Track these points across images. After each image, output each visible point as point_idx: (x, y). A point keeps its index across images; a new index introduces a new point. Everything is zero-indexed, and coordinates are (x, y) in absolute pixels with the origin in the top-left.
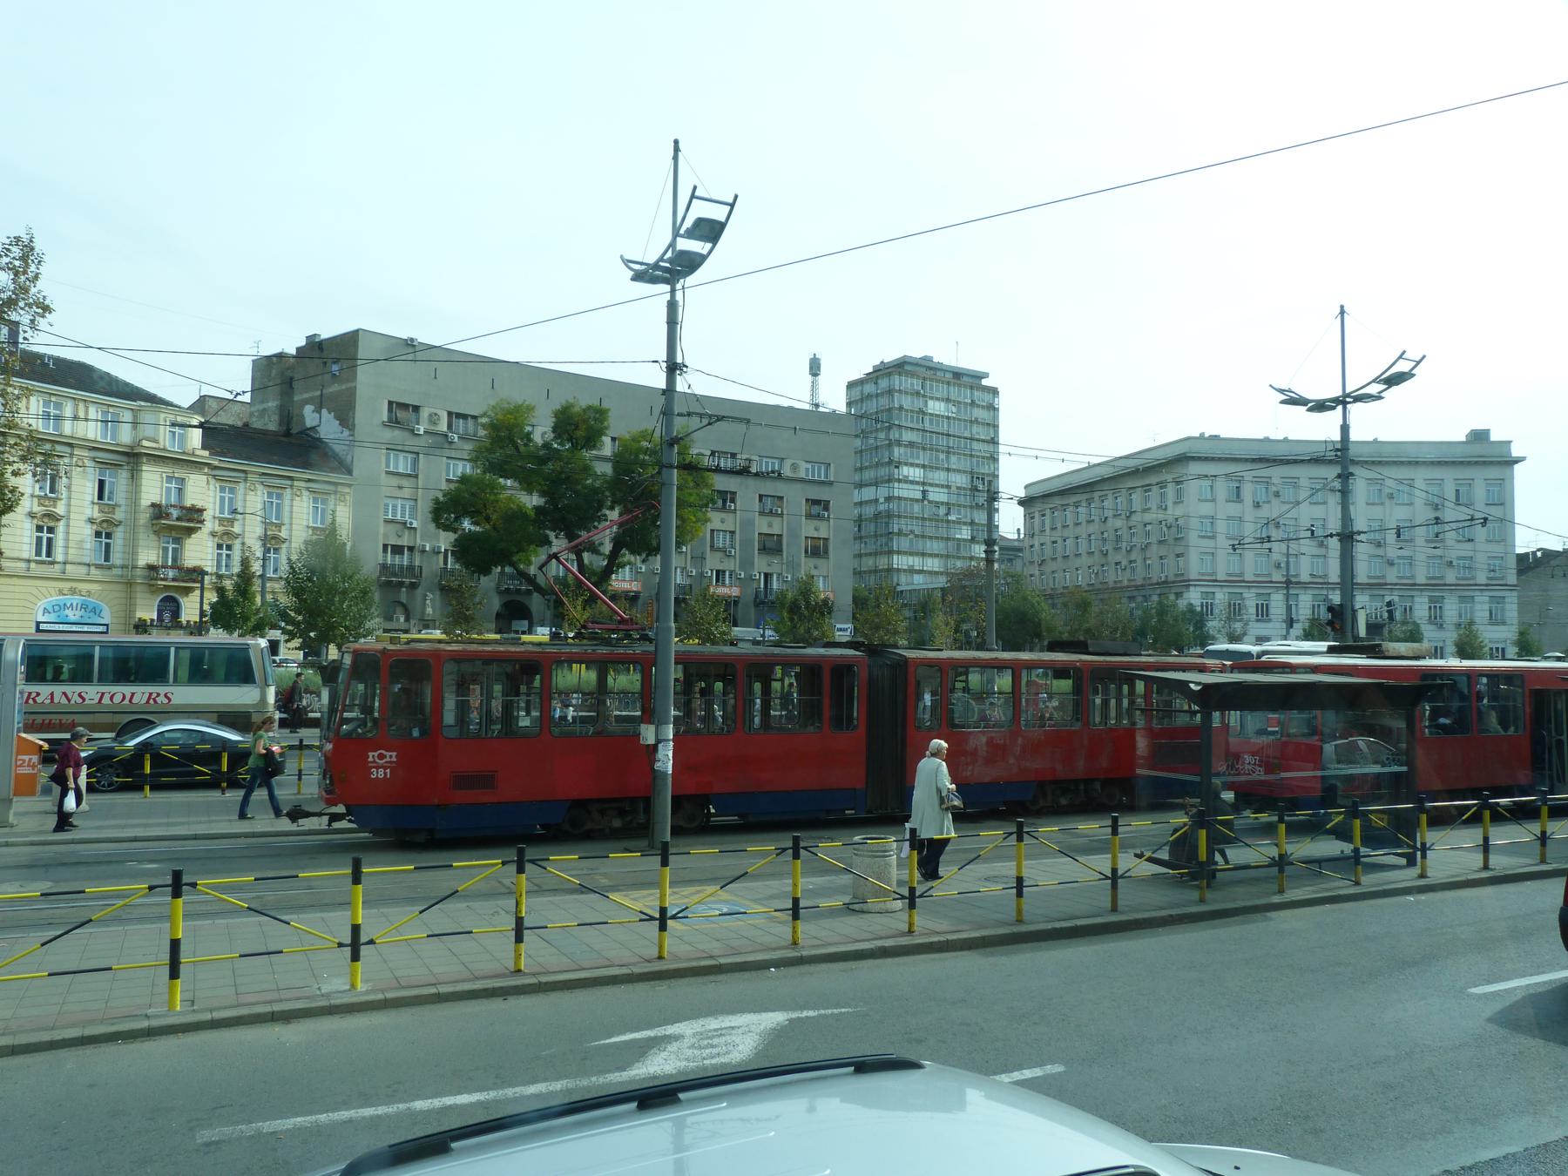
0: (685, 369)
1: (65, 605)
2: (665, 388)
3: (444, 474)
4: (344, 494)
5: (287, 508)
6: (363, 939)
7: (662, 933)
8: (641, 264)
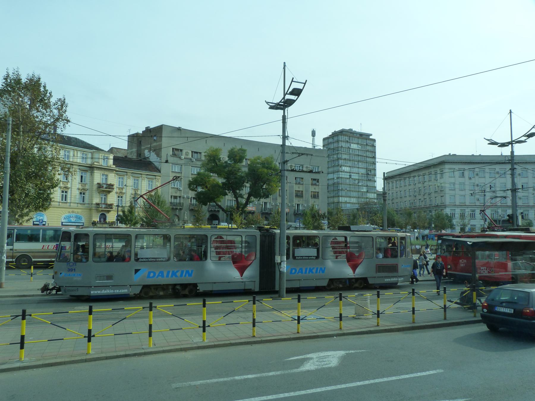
0: (288, 138)
1: (70, 216)
2: (282, 144)
3: (190, 172)
4: (158, 179)
5: (140, 184)
6: (206, 325)
7: (414, 315)
8: (272, 103)
